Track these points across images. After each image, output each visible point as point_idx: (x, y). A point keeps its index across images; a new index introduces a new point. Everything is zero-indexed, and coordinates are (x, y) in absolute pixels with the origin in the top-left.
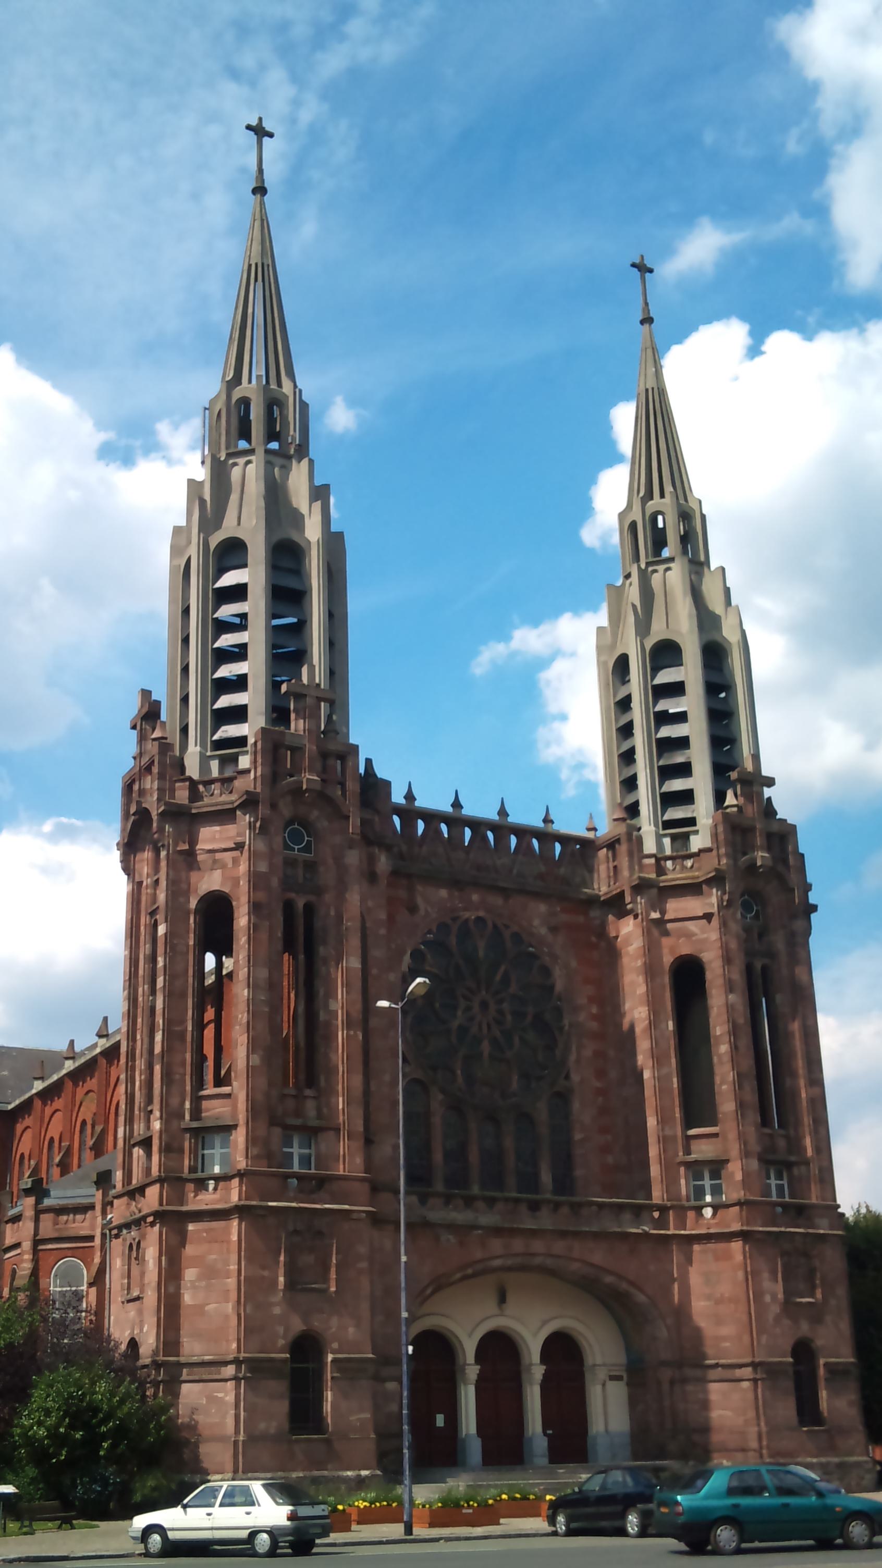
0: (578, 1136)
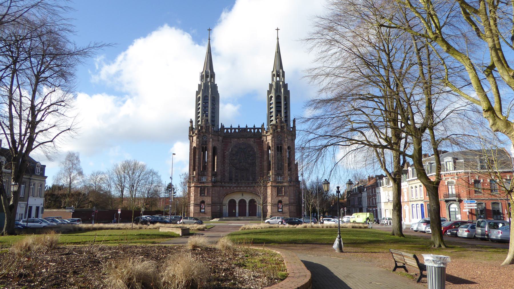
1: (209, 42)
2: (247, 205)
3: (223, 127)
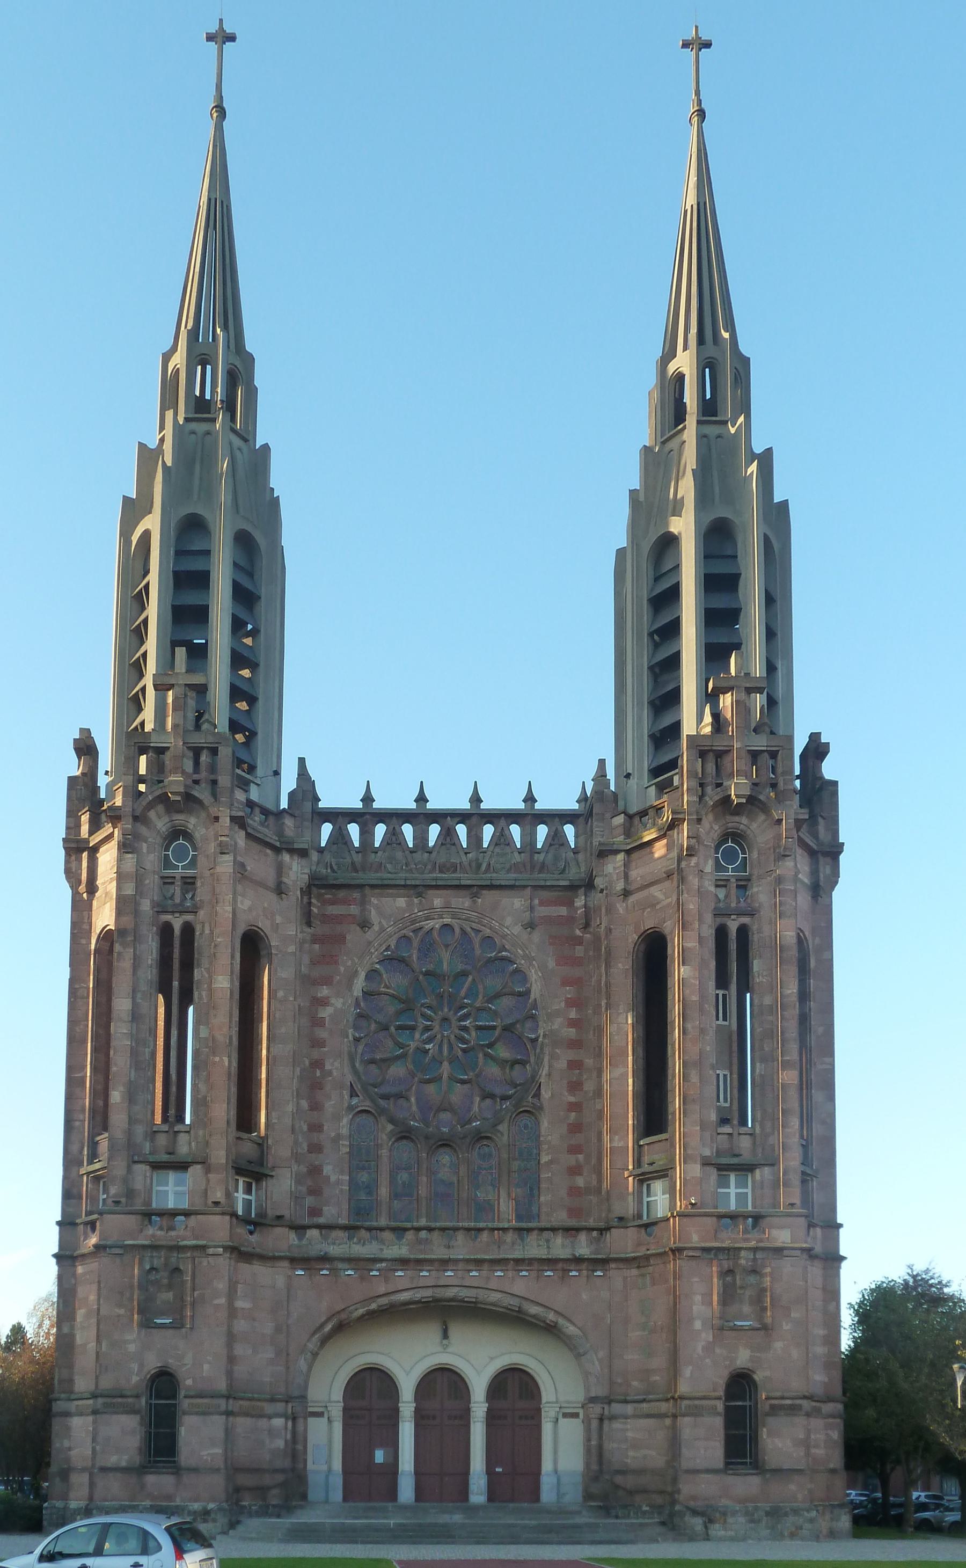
0: (545, 1159)
1: (219, 130)
2: (407, 1408)
3: (306, 787)
